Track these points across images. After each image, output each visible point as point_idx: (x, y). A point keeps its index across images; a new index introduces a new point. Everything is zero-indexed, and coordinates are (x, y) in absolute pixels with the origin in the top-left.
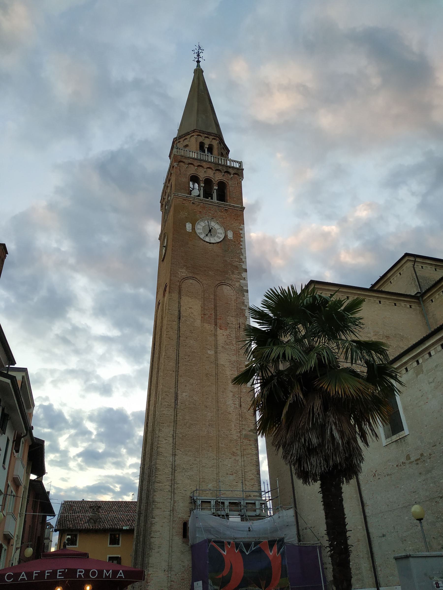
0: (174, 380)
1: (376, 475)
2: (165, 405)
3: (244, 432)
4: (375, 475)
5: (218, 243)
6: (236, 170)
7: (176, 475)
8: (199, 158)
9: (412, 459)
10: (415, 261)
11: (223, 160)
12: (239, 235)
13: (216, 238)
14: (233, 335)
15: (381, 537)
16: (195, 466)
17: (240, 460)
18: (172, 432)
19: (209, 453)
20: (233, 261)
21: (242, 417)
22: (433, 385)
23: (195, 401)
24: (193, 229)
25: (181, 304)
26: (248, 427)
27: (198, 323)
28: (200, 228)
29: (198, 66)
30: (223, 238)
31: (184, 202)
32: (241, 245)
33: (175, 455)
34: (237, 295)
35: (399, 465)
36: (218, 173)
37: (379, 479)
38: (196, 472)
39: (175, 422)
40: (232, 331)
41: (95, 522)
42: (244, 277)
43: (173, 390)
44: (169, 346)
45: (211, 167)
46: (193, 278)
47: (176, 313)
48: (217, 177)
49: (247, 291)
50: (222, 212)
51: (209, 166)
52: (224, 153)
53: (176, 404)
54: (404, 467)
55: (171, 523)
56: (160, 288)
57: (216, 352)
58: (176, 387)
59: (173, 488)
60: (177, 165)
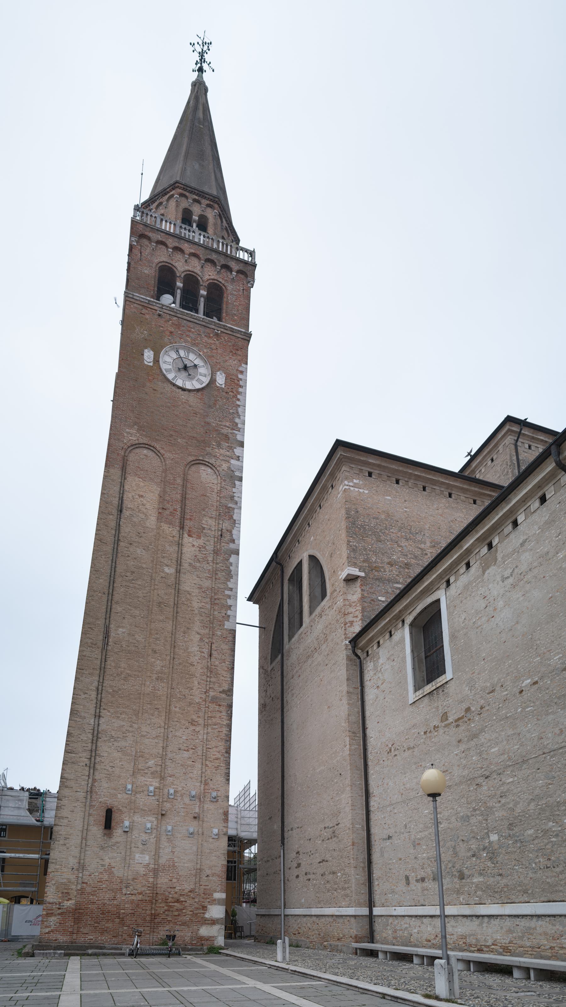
0: (104, 607)
1: (393, 750)
2: (87, 643)
3: (212, 694)
4: (390, 750)
6: (242, 265)
7: (99, 744)
8: (178, 232)
9: (451, 719)
11: (221, 244)
12: (236, 381)
13: (194, 382)
14: (210, 548)
15: (386, 839)
16: (131, 734)
19: (153, 718)
20: (221, 425)
21: (211, 672)
22: (511, 580)
23: (138, 641)
24: (156, 360)
25: (126, 487)
26: (220, 687)
27: (152, 521)
28: (168, 361)
29: (200, 77)
30: (207, 382)
31: (144, 311)
32: (239, 400)
33: (99, 716)
34: (223, 483)
35: (429, 731)
37: (396, 755)
38: (131, 742)
39: (103, 669)
40: (208, 541)
42: (237, 454)
43: (101, 622)
45: (198, 252)
46: (148, 447)
47: (116, 501)
48: (208, 274)
49: (240, 479)
50: (210, 337)
51: (193, 251)
53: (106, 642)
54: (436, 734)
55: (88, 808)
57: (178, 571)
59: (93, 762)
60: (137, 242)
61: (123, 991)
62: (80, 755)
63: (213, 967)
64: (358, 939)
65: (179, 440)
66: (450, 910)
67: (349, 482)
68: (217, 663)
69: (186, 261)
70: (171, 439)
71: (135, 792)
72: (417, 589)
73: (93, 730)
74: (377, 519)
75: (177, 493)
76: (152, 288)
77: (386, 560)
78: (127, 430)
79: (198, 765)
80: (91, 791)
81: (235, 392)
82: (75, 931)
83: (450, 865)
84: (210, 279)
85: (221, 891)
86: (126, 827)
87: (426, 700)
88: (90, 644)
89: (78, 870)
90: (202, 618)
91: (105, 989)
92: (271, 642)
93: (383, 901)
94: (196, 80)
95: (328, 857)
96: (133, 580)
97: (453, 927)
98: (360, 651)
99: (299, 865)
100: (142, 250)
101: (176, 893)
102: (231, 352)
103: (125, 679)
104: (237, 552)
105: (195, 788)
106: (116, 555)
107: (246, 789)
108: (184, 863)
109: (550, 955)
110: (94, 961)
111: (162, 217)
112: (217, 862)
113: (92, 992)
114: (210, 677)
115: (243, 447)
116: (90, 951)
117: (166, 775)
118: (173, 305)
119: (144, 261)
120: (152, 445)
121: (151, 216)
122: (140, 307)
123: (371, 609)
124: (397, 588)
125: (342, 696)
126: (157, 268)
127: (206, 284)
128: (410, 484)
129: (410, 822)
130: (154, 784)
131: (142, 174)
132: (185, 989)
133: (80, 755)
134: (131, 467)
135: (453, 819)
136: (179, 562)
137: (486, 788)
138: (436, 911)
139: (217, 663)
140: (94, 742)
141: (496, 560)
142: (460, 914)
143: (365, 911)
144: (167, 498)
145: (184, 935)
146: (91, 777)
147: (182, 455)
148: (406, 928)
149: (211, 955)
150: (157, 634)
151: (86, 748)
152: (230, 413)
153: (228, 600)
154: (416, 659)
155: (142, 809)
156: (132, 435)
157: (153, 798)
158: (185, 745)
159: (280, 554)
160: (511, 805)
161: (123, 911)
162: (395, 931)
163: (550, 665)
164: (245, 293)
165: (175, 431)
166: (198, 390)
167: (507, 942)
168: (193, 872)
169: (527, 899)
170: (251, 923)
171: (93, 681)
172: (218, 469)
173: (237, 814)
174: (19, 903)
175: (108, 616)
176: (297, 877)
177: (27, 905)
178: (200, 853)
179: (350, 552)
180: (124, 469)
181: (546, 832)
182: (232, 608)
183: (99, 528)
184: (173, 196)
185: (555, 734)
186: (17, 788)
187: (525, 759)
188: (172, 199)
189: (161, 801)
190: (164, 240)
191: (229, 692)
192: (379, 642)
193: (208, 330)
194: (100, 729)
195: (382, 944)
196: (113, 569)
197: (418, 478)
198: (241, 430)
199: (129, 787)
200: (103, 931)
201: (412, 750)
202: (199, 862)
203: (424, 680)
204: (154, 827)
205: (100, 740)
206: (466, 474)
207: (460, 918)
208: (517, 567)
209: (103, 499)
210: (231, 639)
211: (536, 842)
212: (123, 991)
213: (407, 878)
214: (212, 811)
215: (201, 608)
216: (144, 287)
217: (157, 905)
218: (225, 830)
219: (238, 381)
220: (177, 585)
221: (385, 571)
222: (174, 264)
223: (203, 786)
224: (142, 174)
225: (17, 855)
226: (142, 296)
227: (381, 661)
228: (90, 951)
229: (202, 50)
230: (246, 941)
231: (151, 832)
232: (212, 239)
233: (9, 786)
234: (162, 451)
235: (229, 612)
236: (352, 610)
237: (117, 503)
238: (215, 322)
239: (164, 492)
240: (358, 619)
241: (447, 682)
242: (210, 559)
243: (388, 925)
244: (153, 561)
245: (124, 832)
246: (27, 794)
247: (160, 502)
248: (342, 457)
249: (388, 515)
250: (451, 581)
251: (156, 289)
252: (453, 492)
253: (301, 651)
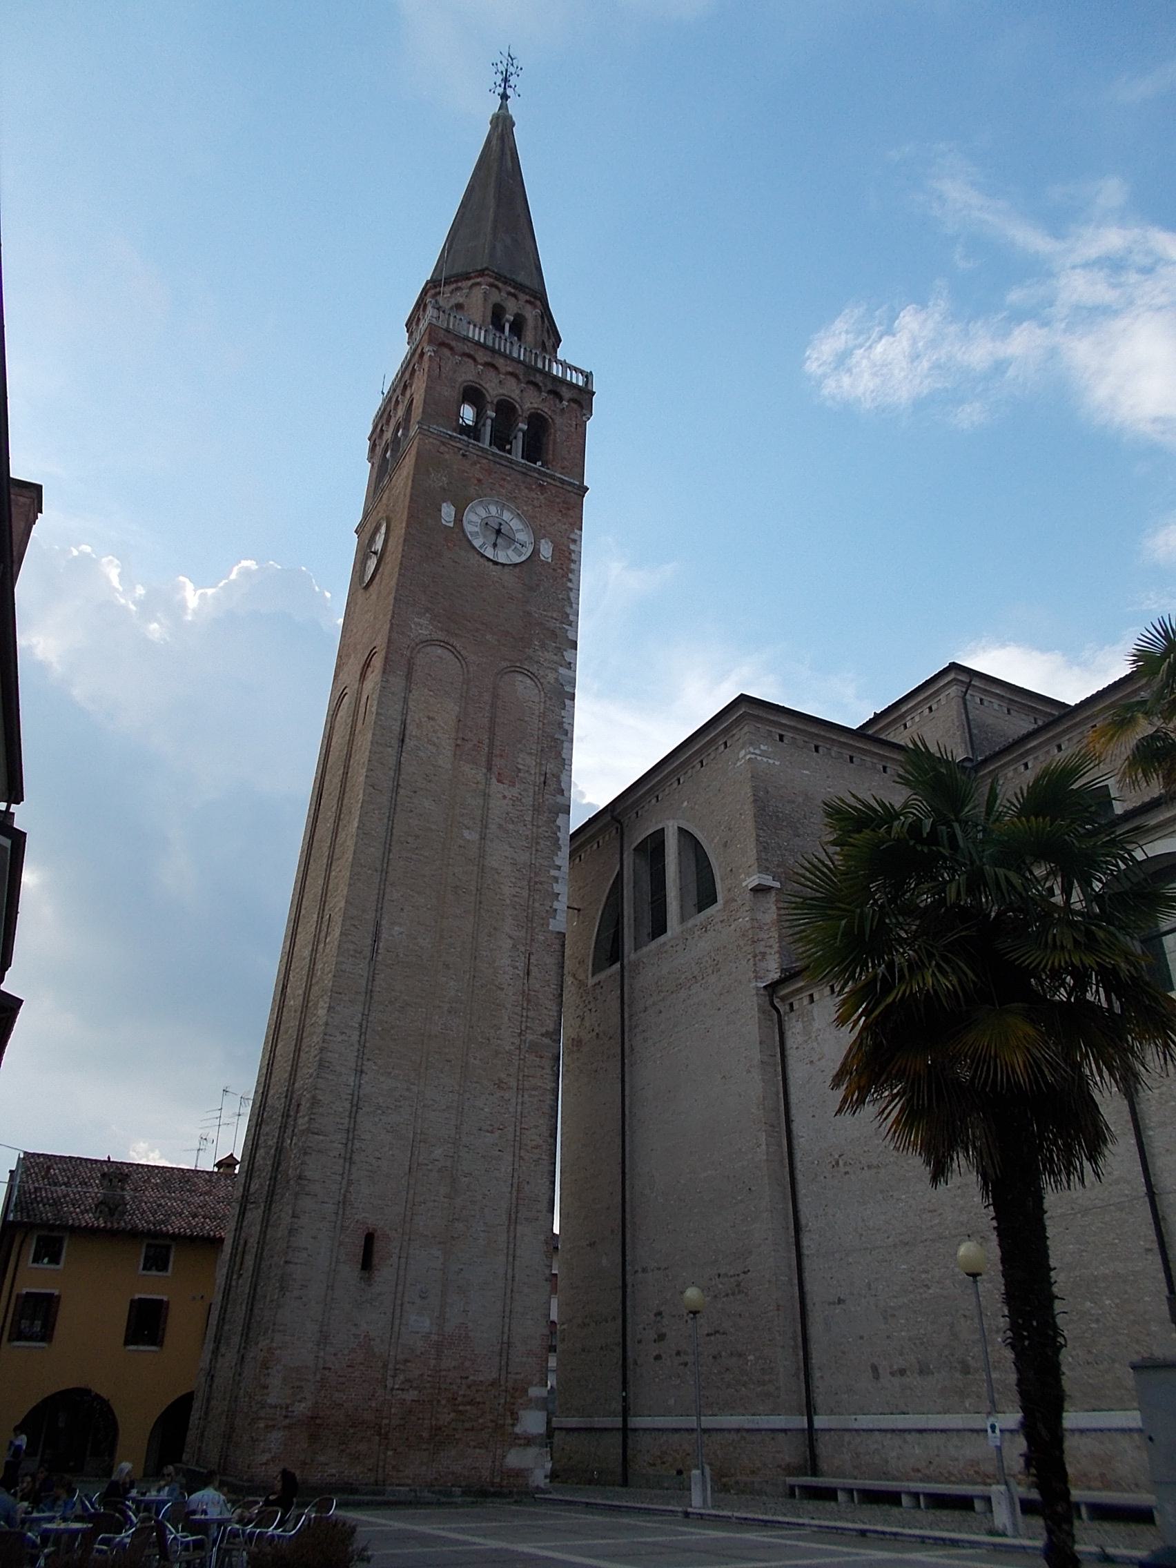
1: (841, 1163)
2: (348, 950)
3: (530, 1037)
4: (837, 1163)
5: (516, 565)
7: (359, 1120)
10: (969, 685)
13: (510, 552)
14: (528, 801)
15: (834, 1303)
21: (529, 1001)
24: (459, 519)
28: (473, 519)
29: (503, 107)
31: (442, 449)
33: (362, 1072)
36: (531, 392)
37: (846, 1173)
39: (370, 993)
41: (112, 1212)
43: (370, 916)
44: (372, 807)
46: (445, 644)
47: (397, 727)
48: (530, 402)
50: (531, 490)
52: (549, 344)
53: (375, 951)
56: (349, 656)
57: (483, 838)
58: (379, 909)
64: (791, 1470)
65: (488, 637)
74: (794, 802)
83: (946, 1352)
99: (661, 1337)
114: (528, 1010)
127: (526, 414)
180: (409, 676)
184: (479, 284)
193: (528, 479)
198: (573, 625)
201: (875, 1170)
213: (875, 1369)
227: (816, 1025)
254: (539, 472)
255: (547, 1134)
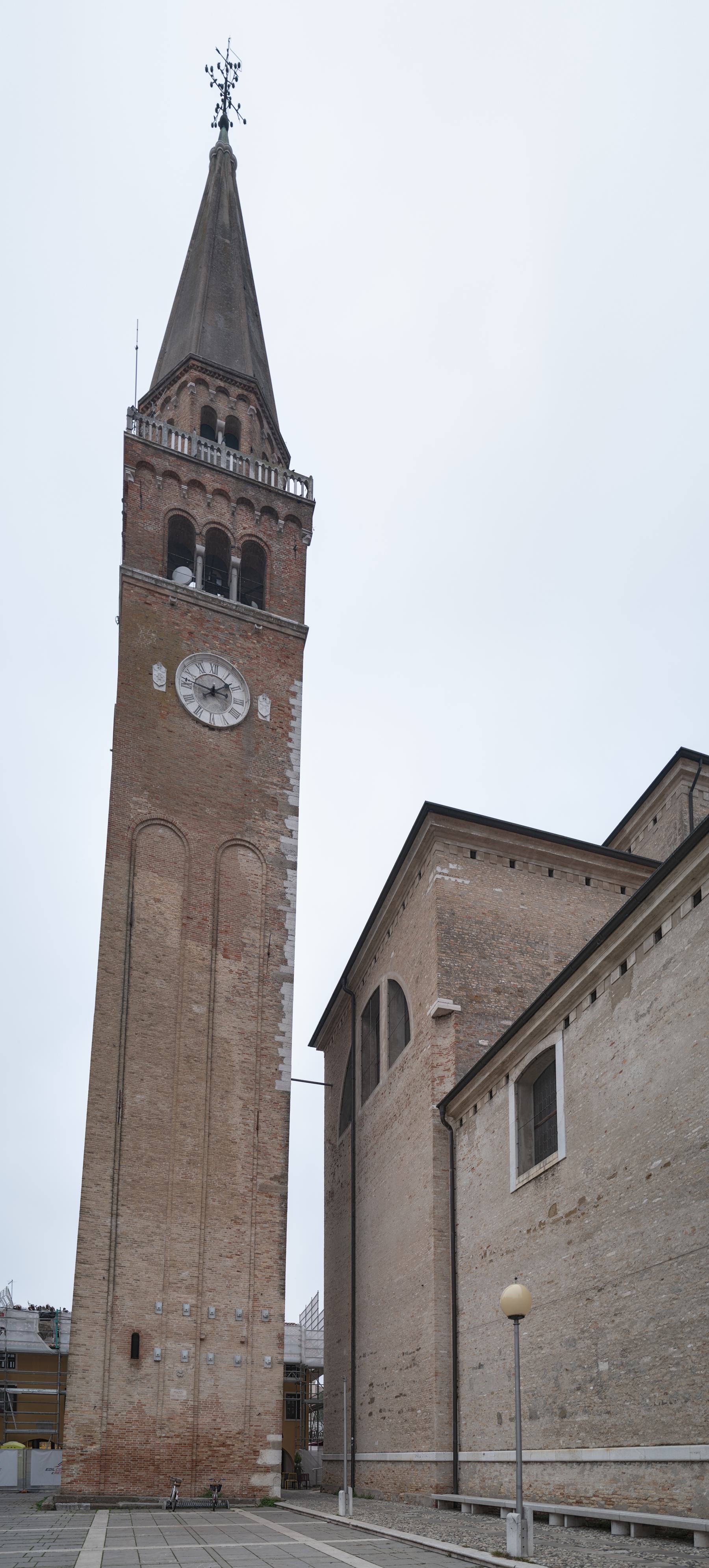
0: (116, 1065)
1: (488, 1253)
2: (95, 1116)
3: (260, 1181)
4: (485, 1254)
7: (119, 1251)
9: (560, 1213)
12: (286, 710)
13: (227, 715)
14: (254, 973)
15: (476, 1368)
17: (248, 1232)
18: (110, 1172)
20: (266, 782)
21: (259, 1151)
22: (647, 1019)
23: (162, 1112)
24: (171, 682)
27: (173, 938)
29: (223, 137)
30: (245, 714)
31: (150, 599)
33: (117, 1215)
34: (270, 874)
35: (533, 1228)
36: (243, 515)
37: (491, 1261)
39: (118, 1152)
40: (251, 963)
42: (289, 827)
43: (112, 1087)
45: (226, 488)
47: (123, 910)
48: (243, 526)
49: (294, 866)
50: (247, 638)
53: (120, 1116)
54: (541, 1232)
55: (109, 1333)
57: (211, 1011)
59: (112, 1275)
60: (135, 476)
61: (152, 1547)
62: (96, 1265)
63: (262, 1521)
64: (439, 1490)
65: (208, 810)
66: (526, 1456)
67: (442, 868)
68: (266, 1138)
69: (209, 504)
70: (195, 808)
71: (166, 1311)
72: (526, 1031)
73: (111, 1233)
74: (481, 923)
75: (206, 893)
76: (160, 558)
77: (492, 985)
78: (134, 798)
79: (245, 1276)
80: (111, 1312)
81: (285, 728)
82: (102, 1481)
83: (550, 1401)
84: (245, 535)
85: (276, 1433)
86: (158, 1356)
87: (531, 1187)
88: (99, 1118)
89: (101, 1408)
90: (244, 1076)
91: (132, 1546)
92: (339, 1106)
93: (471, 1444)
94: (218, 145)
95: (406, 1390)
96: (151, 1025)
97: (550, 1475)
98: (452, 1118)
99: (372, 1400)
100: (143, 491)
101: (221, 1435)
102: (279, 660)
103: (148, 1164)
104: (290, 979)
105: (241, 1305)
106: (128, 990)
107: (314, 1303)
108: (230, 1399)
109: (658, 1508)
110: (125, 1515)
111: (170, 427)
112: (270, 1395)
113: (116, 1549)
114: (258, 1159)
115: (298, 815)
116: (121, 1504)
117: (205, 1289)
118: (192, 585)
119: (146, 511)
120: (170, 819)
121: (154, 426)
122: (143, 592)
123: (468, 1058)
124: (505, 1026)
125: (427, 1182)
126: (166, 522)
127: (239, 545)
128: (530, 866)
129: (506, 1346)
130: (189, 1301)
131: (137, 348)
132: (223, 1545)
133: (96, 1265)
134: (141, 857)
135: (557, 1343)
136: (212, 996)
137: (597, 1304)
138: (512, 1456)
139: (266, 1138)
140: (113, 1248)
141: (630, 988)
142: (558, 1459)
143: (449, 1456)
144: (193, 901)
145: (232, 1484)
146: (111, 1293)
147: (212, 833)
148: (496, 1476)
149: (265, 1508)
150: (186, 1101)
151: (103, 1257)
152: (278, 762)
153: (279, 1049)
154: (522, 1130)
155: (176, 1334)
156: (141, 807)
157: (189, 1319)
158: (228, 1250)
159: (350, 978)
160: (626, 1326)
161: (158, 1457)
162: (483, 1480)
163: (686, 1140)
164: (299, 555)
165: (202, 797)
166: (232, 728)
167: (611, 1492)
168: (242, 1410)
169: (636, 1442)
170: (317, 1471)
171: (106, 1168)
172: (262, 851)
173: (301, 1336)
174: (38, 1448)
175: (121, 1077)
176: (371, 1414)
177: (47, 1450)
178: (249, 1387)
179: (442, 975)
180: (132, 859)
181: (665, 1359)
182: (285, 1061)
183: (103, 952)
185: (686, 1233)
186: (25, 1306)
187: (648, 1266)
188: (185, 389)
189: (199, 1322)
190: (174, 469)
191: (283, 1178)
192: (475, 1106)
193: (244, 626)
194: (118, 1232)
195: (468, 1495)
196: (125, 1011)
197: (542, 856)
198: (294, 789)
199: (159, 1305)
200: (136, 1481)
202: (248, 1397)
203: (531, 1159)
204: (192, 1355)
205: (119, 1246)
206: (614, 847)
207: (559, 1464)
208: (656, 999)
209: (107, 908)
210: (283, 1104)
211: (652, 1372)
212: (152, 1547)
213: (499, 1416)
214: (263, 1334)
215: (243, 1062)
216: (148, 557)
217: (199, 1450)
218: (280, 1357)
219: (290, 709)
220: (210, 1030)
221: (489, 1002)
222: (190, 512)
223: (251, 1302)
224: (137, 348)
225: (31, 1390)
226: (146, 573)
227: (478, 1133)
228: (121, 1504)
229: (226, 79)
230: (312, 1492)
231: (188, 1362)
232: (247, 461)
233: (16, 1303)
234: (184, 829)
235: (281, 1067)
236: (442, 1060)
237: (125, 912)
238: (253, 611)
239: (189, 892)
240: (450, 1074)
241: (558, 1163)
242: (254, 990)
243: (475, 1473)
244: (177, 997)
245: (156, 1361)
246: (37, 1316)
247: (184, 908)
248: (433, 828)
249: (497, 917)
250: (571, 1019)
251: (166, 559)
252: (593, 876)
253: (378, 1118)
254: (256, 615)
255: (277, 1257)
